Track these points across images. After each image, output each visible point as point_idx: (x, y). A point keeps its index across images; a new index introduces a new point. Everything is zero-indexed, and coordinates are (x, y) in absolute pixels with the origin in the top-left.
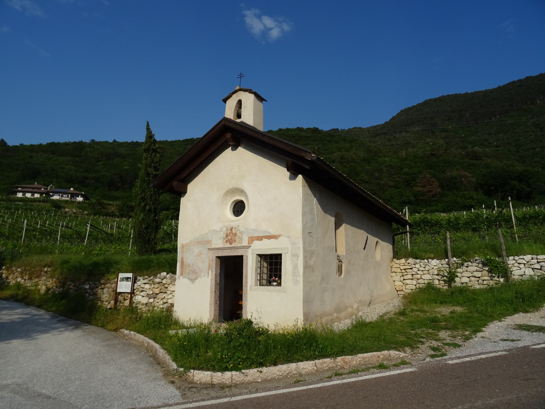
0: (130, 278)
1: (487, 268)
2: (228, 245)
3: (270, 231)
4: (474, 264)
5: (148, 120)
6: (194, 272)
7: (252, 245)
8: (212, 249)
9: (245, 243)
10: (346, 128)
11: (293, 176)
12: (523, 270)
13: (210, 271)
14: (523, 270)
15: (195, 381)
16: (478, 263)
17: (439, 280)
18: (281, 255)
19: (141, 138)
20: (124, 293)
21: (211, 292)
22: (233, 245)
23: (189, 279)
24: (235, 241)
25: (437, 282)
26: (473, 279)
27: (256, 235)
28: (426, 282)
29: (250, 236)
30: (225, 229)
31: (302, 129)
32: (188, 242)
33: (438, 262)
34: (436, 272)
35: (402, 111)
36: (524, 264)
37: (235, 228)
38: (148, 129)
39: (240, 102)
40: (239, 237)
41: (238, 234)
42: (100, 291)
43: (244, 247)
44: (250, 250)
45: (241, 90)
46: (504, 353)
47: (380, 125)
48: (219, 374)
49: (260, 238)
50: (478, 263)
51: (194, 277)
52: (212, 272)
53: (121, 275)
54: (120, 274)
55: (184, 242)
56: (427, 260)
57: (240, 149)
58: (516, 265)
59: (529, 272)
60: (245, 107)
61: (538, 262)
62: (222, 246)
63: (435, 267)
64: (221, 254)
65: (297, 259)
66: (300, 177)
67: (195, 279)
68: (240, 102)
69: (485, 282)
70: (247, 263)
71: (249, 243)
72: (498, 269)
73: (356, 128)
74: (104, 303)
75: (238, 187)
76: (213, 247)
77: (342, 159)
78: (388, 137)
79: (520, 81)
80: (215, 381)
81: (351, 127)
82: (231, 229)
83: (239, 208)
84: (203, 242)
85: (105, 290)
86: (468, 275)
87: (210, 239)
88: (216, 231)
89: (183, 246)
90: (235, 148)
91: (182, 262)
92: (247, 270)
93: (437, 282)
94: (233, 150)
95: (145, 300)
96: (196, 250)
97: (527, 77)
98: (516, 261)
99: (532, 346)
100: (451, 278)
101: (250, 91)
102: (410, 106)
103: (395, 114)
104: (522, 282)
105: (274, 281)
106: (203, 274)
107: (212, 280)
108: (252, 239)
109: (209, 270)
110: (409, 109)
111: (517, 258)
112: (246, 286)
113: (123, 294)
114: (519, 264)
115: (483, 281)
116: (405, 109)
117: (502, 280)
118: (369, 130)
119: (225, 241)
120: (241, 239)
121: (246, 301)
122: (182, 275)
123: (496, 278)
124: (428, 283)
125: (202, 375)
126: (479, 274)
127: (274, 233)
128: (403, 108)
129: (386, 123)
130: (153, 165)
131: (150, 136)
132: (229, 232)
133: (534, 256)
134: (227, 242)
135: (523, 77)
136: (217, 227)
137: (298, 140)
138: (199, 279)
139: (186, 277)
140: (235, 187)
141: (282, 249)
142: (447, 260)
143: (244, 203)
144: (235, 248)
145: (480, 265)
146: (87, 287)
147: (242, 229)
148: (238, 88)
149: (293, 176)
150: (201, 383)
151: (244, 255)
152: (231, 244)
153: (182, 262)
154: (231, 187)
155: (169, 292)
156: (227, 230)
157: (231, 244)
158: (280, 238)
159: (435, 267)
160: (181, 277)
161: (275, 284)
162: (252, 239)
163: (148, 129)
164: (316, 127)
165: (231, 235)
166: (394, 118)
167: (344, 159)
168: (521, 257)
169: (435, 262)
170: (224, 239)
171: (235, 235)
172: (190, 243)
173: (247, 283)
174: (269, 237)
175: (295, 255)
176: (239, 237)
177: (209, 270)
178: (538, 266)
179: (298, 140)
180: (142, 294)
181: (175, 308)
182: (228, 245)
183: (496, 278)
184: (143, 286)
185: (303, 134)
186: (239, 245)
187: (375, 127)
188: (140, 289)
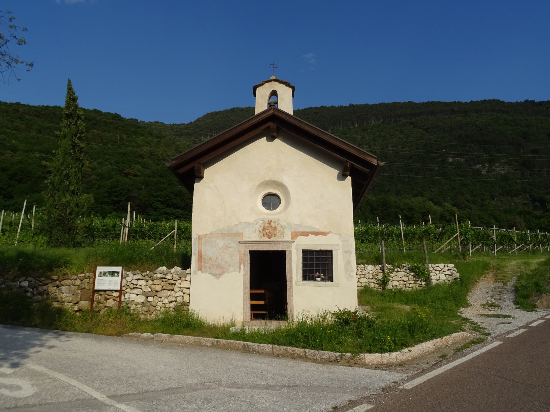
0: (118, 273)
1: (412, 274)
2: (266, 239)
3: (317, 227)
4: (403, 270)
5: (70, 78)
6: (219, 266)
7: (296, 240)
8: (245, 242)
9: (288, 237)
10: (147, 121)
11: (342, 176)
12: (438, 275)
13: (242, 266)
14: (438, 275)
15: (367, 363)
16: (406, 270)
17: (374, 283)
18: (331, 251)
19: (59, 100)
20: (105, 291)
21: (245, 288)
22: (272, 239)
23: (212, 274)
24: (275, 235)
25: (372, 285)
26: (402, 282)
27: (301, 230)
28: (363, 285)
29: (293, 231)
30: (261, 222)
31: (101, 112)
32: (208, 233)
33: (373, 267)
34: (371, 277)
35: (208, 114)
36: (439, 271)
37: (275, 222)
38: (70, 89)
39: (274, 93)
40: (280, 231)
41: (278, 227)
42: (52, 289)
43: (287, 242)
44: (293, 246)
45: (275, 80)
46: (522, 331)
47: (184, 124)
48: (387, 354)
49: (306, 234)
50: (406, 270)
51: (218, 270)
52: (244, 266)
53: (100, 269)
54: (98, 268)
55: (202, 233)
56: (364, 265)
57: (277, 141)
58: (434, 271)
59: (443, 277)
60: (282, 99)
61: (449, 270)
62: (258, 240)
63: (371, 272)
64: (256, 248)
65: (350, 256)
66: (349, 179)
67: (221, 275)
68: (274, 93)
69: (411, 285)
70: (291, 259)
71: (292, 238)
72: (420, 273)
73: (158, 122)
74: (66, 304)
75: (276, 179)
76: (245, 239)
77: (152, 155)
78: (193, 138)
79: (316, 108)
80: (385, 361)
81: (153, 120)
82: (270, 223)
83: (271, 201)
84: (230, 234)
85: (64, 288)
86: (398, 279)
87: (241, 231)
88: (249, 223)
89: (200, 238)
90: (271, 138)
91: (200, 256)
92: (291, 265)
93: (372, 285)
94: (268, 140)
95: (141, 299)
96: (221, 243)
97: (322, 106)
98: (433, 268)
99: (532, 323)
100: (384, 282)
101: (287, 84)
102: (217, 111)
103: (201, 116)
104: (438, 285)
105: (319, 277)
106: (232, 269)
107: (244, 275)
108: (295, 235)
109: (240, 264)
110: (216, 113)
111: (434, 266)
112: (291, 281)
113: (101, 293)
114: (436, 270)
115: (409, 284)
116: (212, 113)
117: (423, 283)
118: (172, 127)
119: (262, 234)
120: (282, 233)
121: (292, 296)
122: (200, 269)
123: (419, 282)
124: (365, 287)
125: (373, 357)
126: (406, 279)
127: (322, 230)
128: (210, 112)
129: (191, 123)
130: (79, 135)
131: (72, 99)
132: (266, 225)
133: (446, 265)
134: (264, 235)
135: (319, 106)
136: (251, 219)
137: (96, 124)
138: (226, 274)
139: (206, 272)
140: (273, 179)
141: (332, 245)
142: (380, 266)
143: (273, 197)
144: (274, 242)
145: (408, 271)
146: (25, 284)
147: (283, 223)
148: (273, 77)
149: (342, 176)
150: (373, 364)
151: (286, 249)
152: (270, 238)
153: (200, 256)
154: (267, 179)
155: (176, 289)
156: (264, 223)
157: (270, 238)
158: (328, 235)
159: (371, 272)
160: (199, 272)
161: (318, 279)
162: (295, 235)
163: (70, 89)
164: (117, 113)
165: (269, 229)
166: (199, 120)
167: (154, 155)
168: (437, 265)
169: (370, 267)
170: (260, 232)
171: (275, 229)
172: (211, 234)
173: (291, 278)
174: (317, 233)
175: (347, 252)
176: (280, 231)
177: (240, 264)
178: (448, 273)
179: (96, 124)
180: (136, 291)
181: (192, 307)
182: (266, 239)
183: (419, 282)
184: (135, 282)
185: (98, 118)
186: (280, 239)
187: (178, 125)
188: (132, 286)
